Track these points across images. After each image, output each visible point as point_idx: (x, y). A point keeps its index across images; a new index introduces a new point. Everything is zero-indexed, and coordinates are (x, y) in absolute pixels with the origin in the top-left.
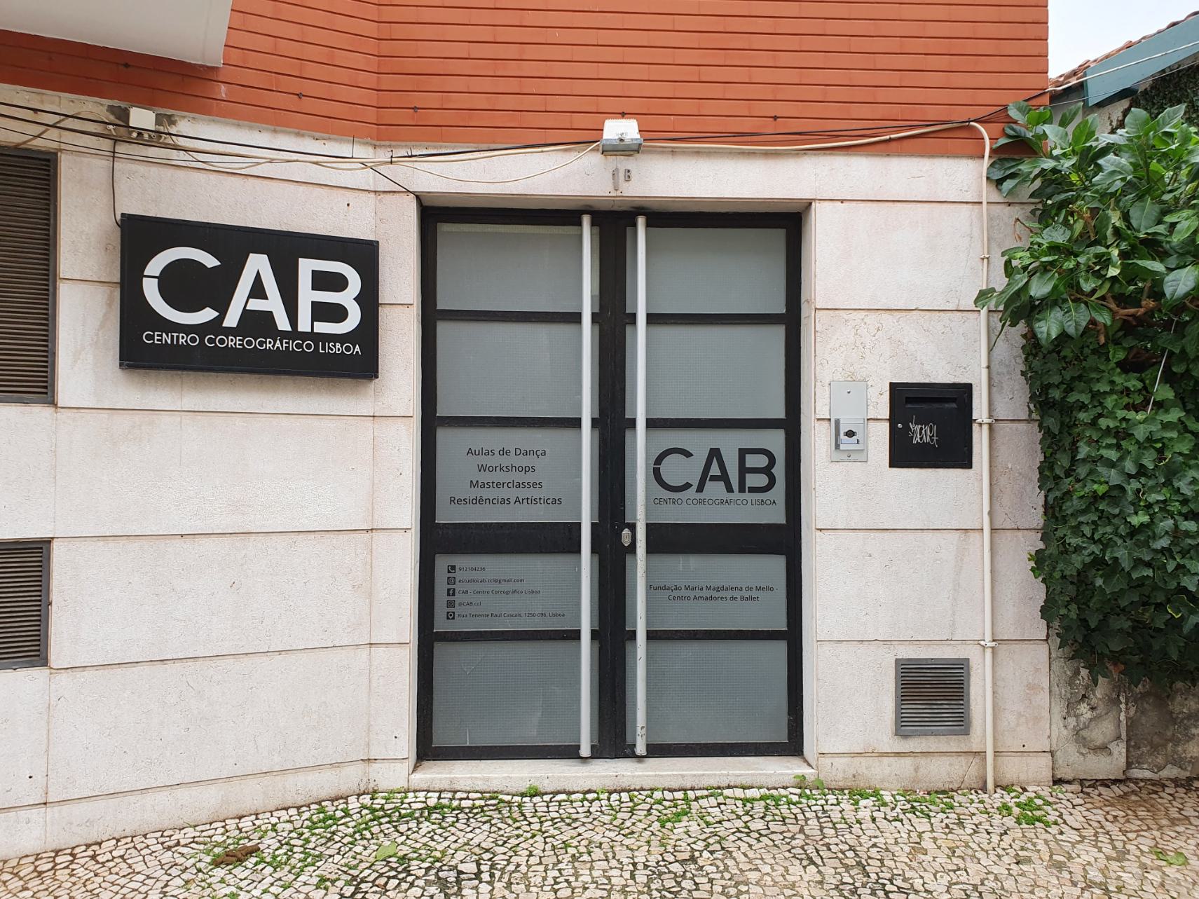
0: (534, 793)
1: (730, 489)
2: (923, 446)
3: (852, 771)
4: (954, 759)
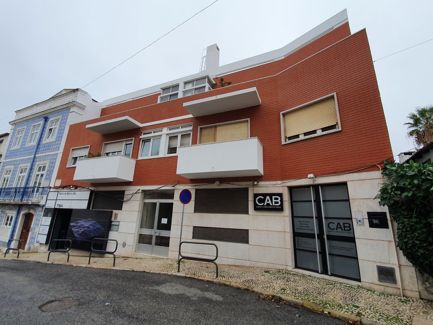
0: (310, 276)
1: (342, 230)
2: (376, 224)
3: (369, 286)
4: (394, 289)
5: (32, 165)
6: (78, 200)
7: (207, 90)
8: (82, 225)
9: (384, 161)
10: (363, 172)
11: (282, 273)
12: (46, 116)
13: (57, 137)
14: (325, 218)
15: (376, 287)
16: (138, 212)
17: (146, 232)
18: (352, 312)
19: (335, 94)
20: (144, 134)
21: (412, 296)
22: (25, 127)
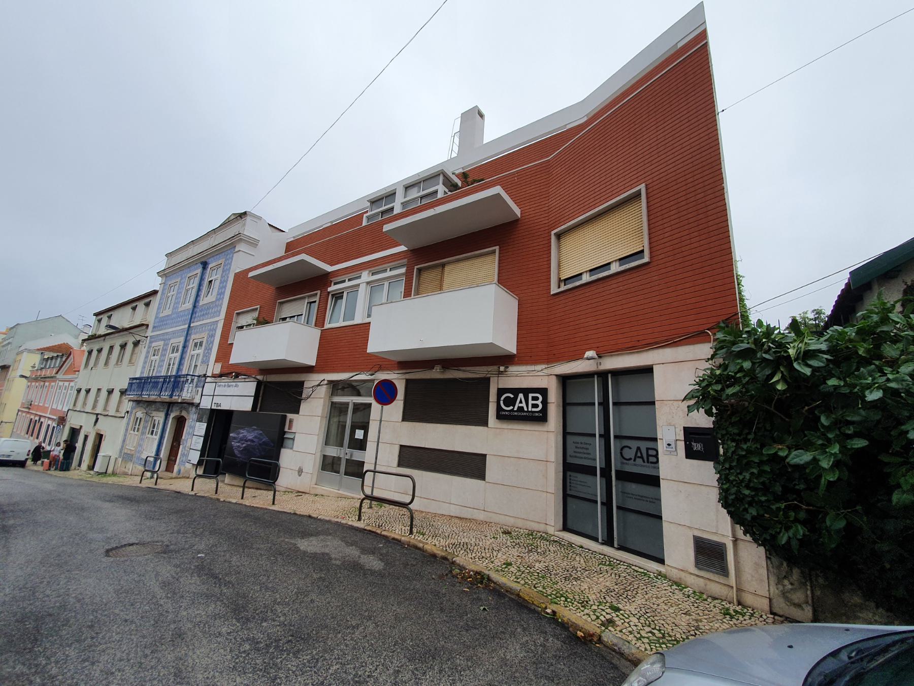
0: (582, 547)
3: (678, 576)
5: (186, 341)
6: (238, 397)
7: (440, 195)
8: (244, 436)
9: (719, 323)
10: (681, 345)
11: (533, 539)
12: (203, 260)
13: (218, 296)
14: (615, 437)
15: (690, 580)
16: (322, 417)
17: (332, 451)
18: (598, 618)
19: (642, 187)
20: (335, 284)
21: (755, 605)
22: (178, 280)
